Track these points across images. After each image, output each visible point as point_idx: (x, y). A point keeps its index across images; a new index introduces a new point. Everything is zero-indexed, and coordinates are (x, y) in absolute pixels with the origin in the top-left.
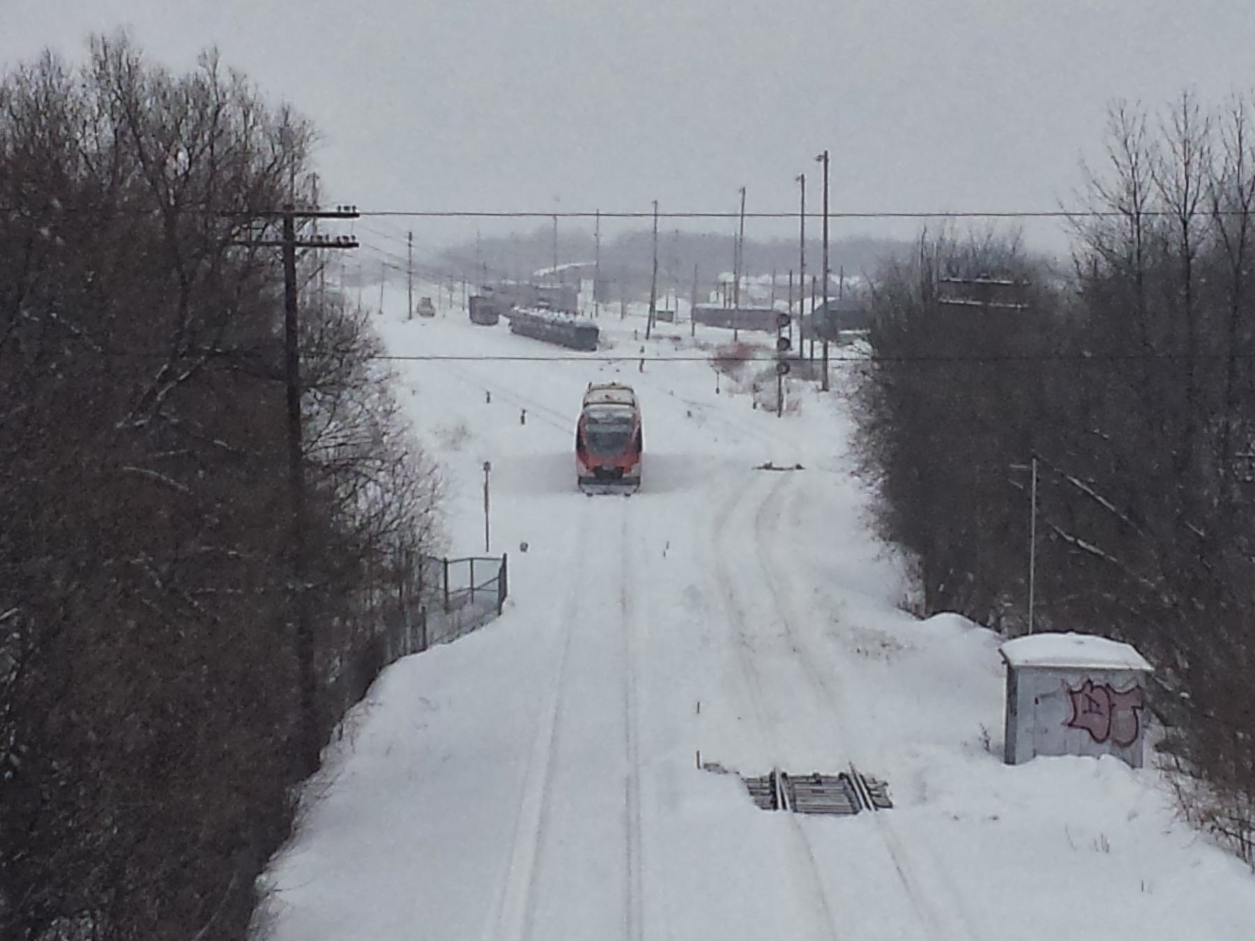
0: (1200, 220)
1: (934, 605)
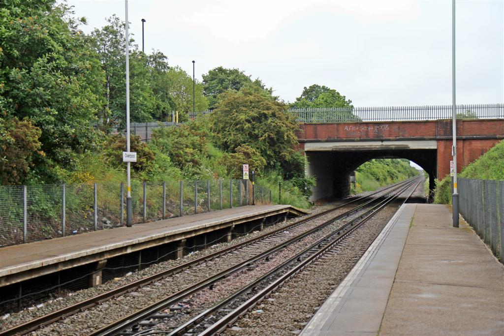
1: (210, 72)
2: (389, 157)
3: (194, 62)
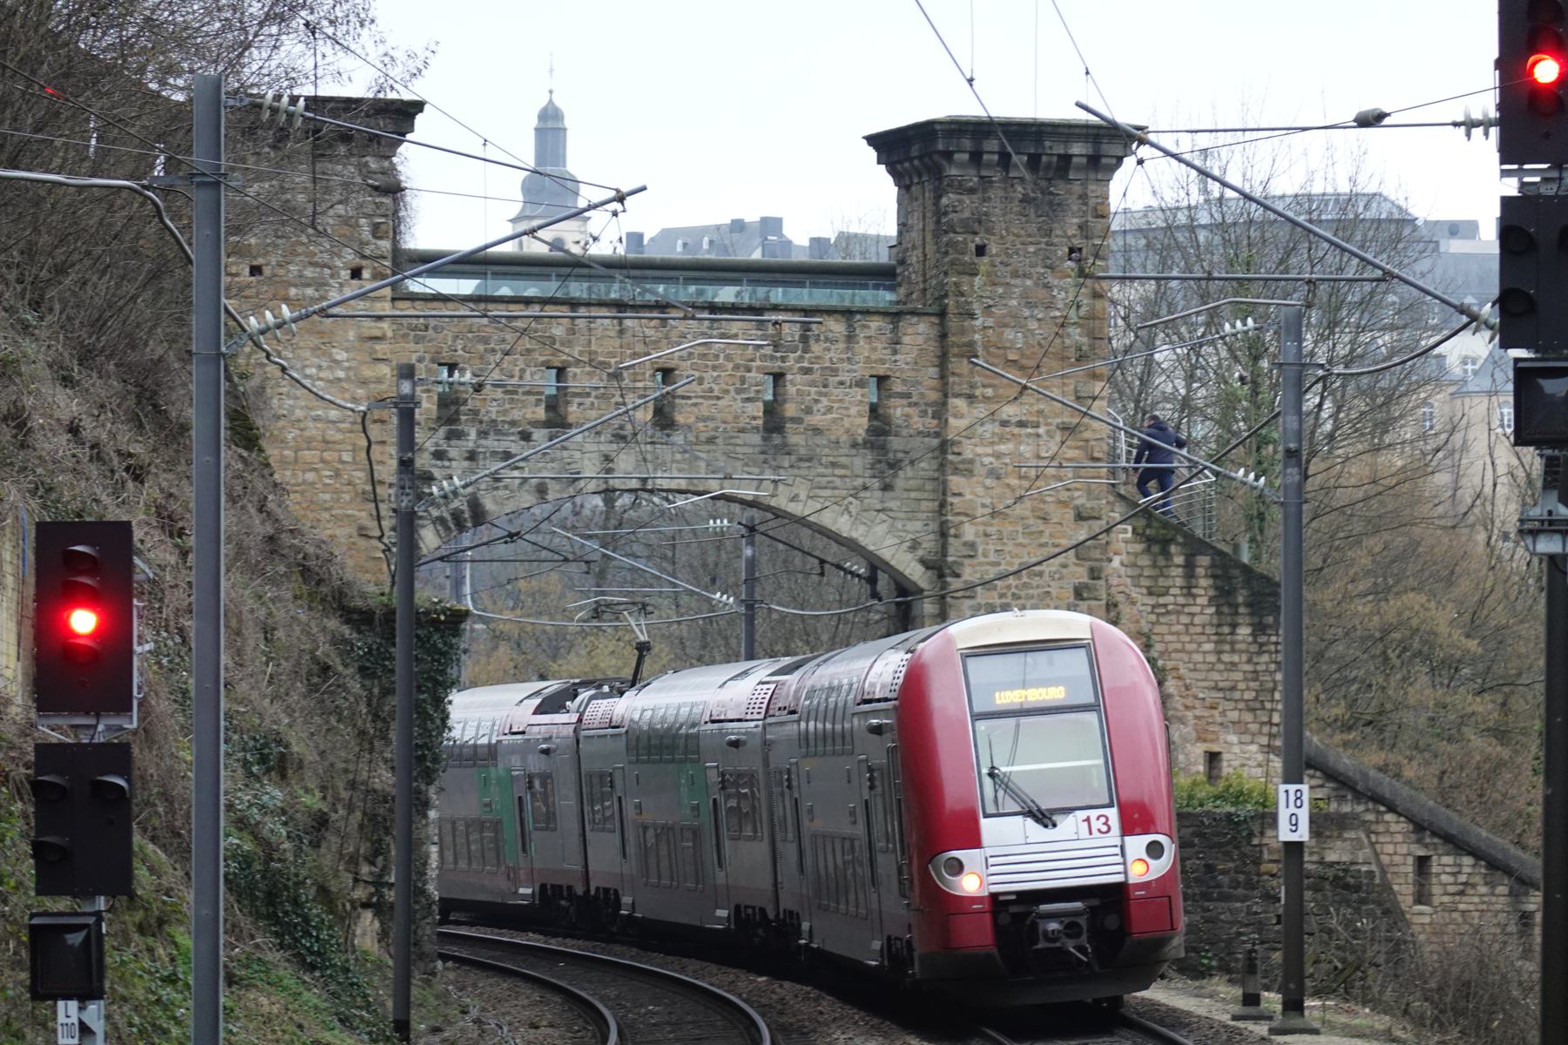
1: (879, 163)
2: (1015, 128)
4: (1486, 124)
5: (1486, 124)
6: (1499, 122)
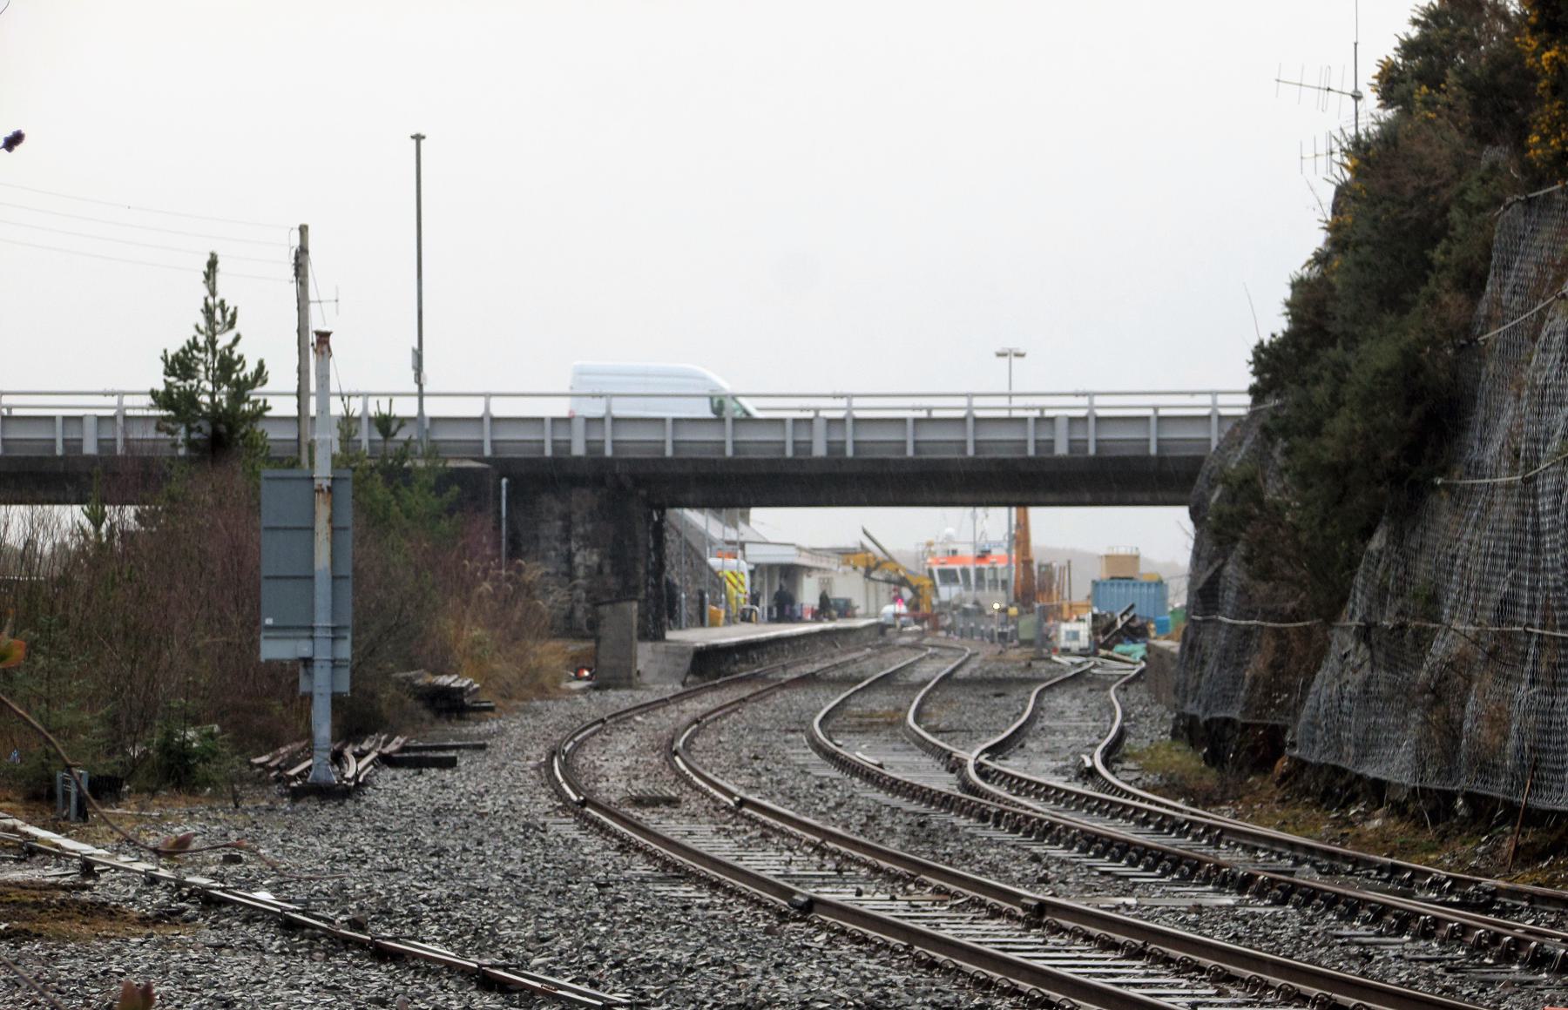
0: (1445, 503)
1: (1293, 286)
3: (418, 138)
4: (347, 412)
5: (347, 412)
6: (1023, 505)
